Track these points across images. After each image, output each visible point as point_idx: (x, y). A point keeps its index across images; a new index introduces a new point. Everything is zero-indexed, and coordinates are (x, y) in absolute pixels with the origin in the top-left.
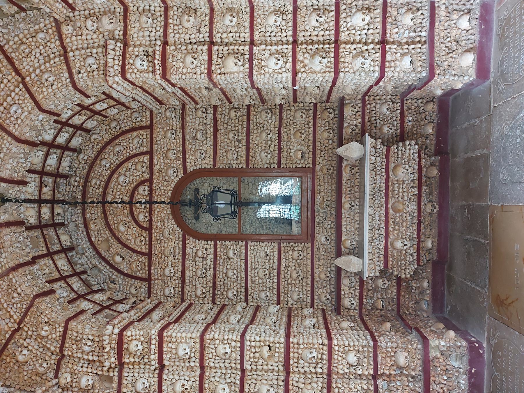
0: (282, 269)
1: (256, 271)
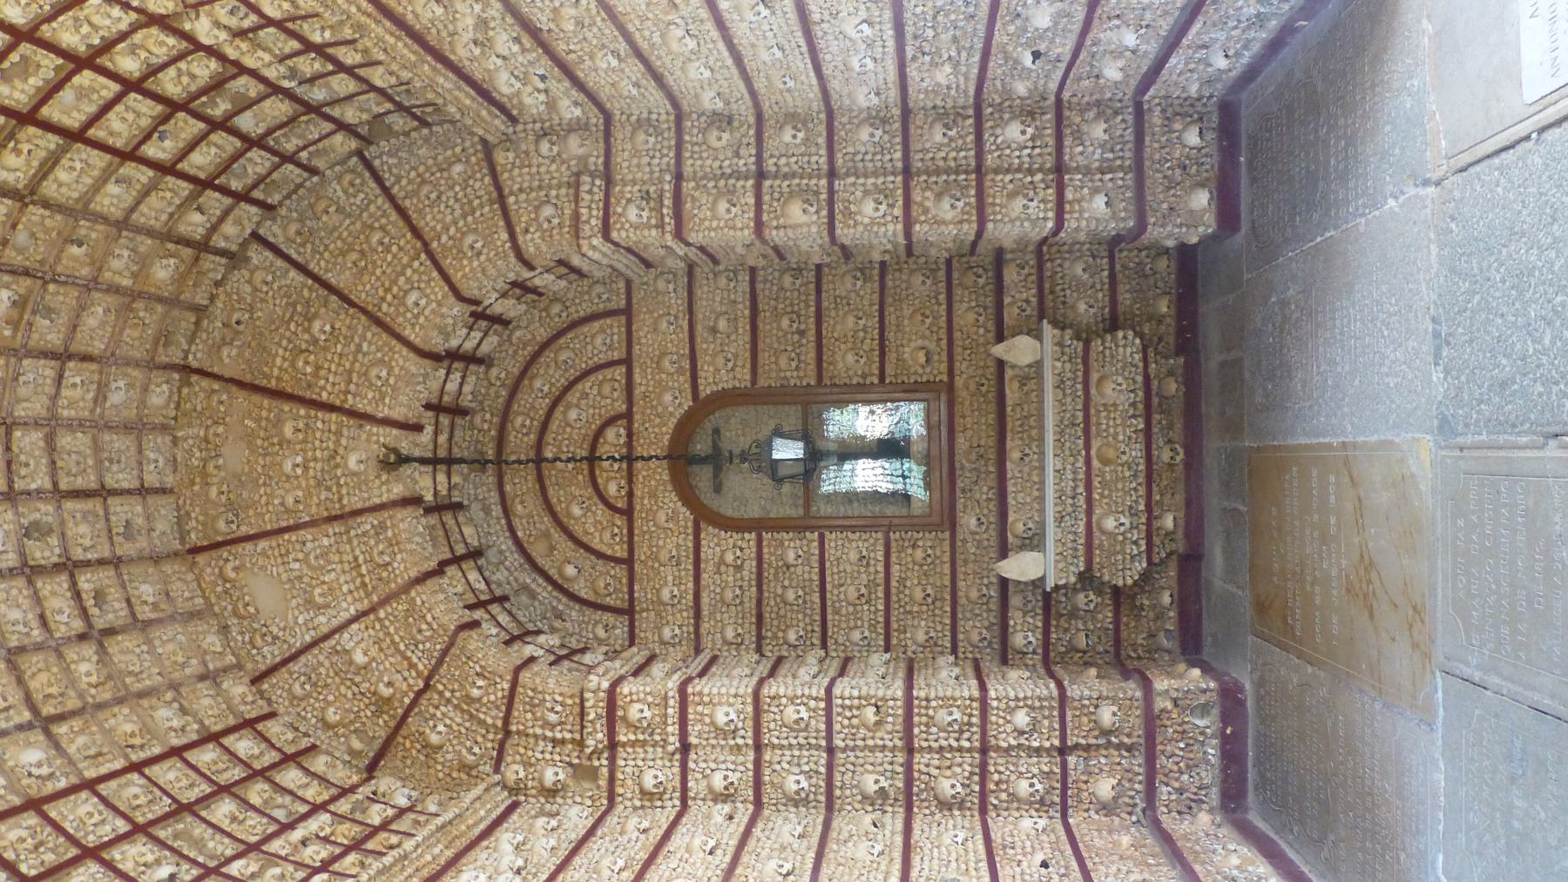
0: (894, 584)
1: (842, 589)
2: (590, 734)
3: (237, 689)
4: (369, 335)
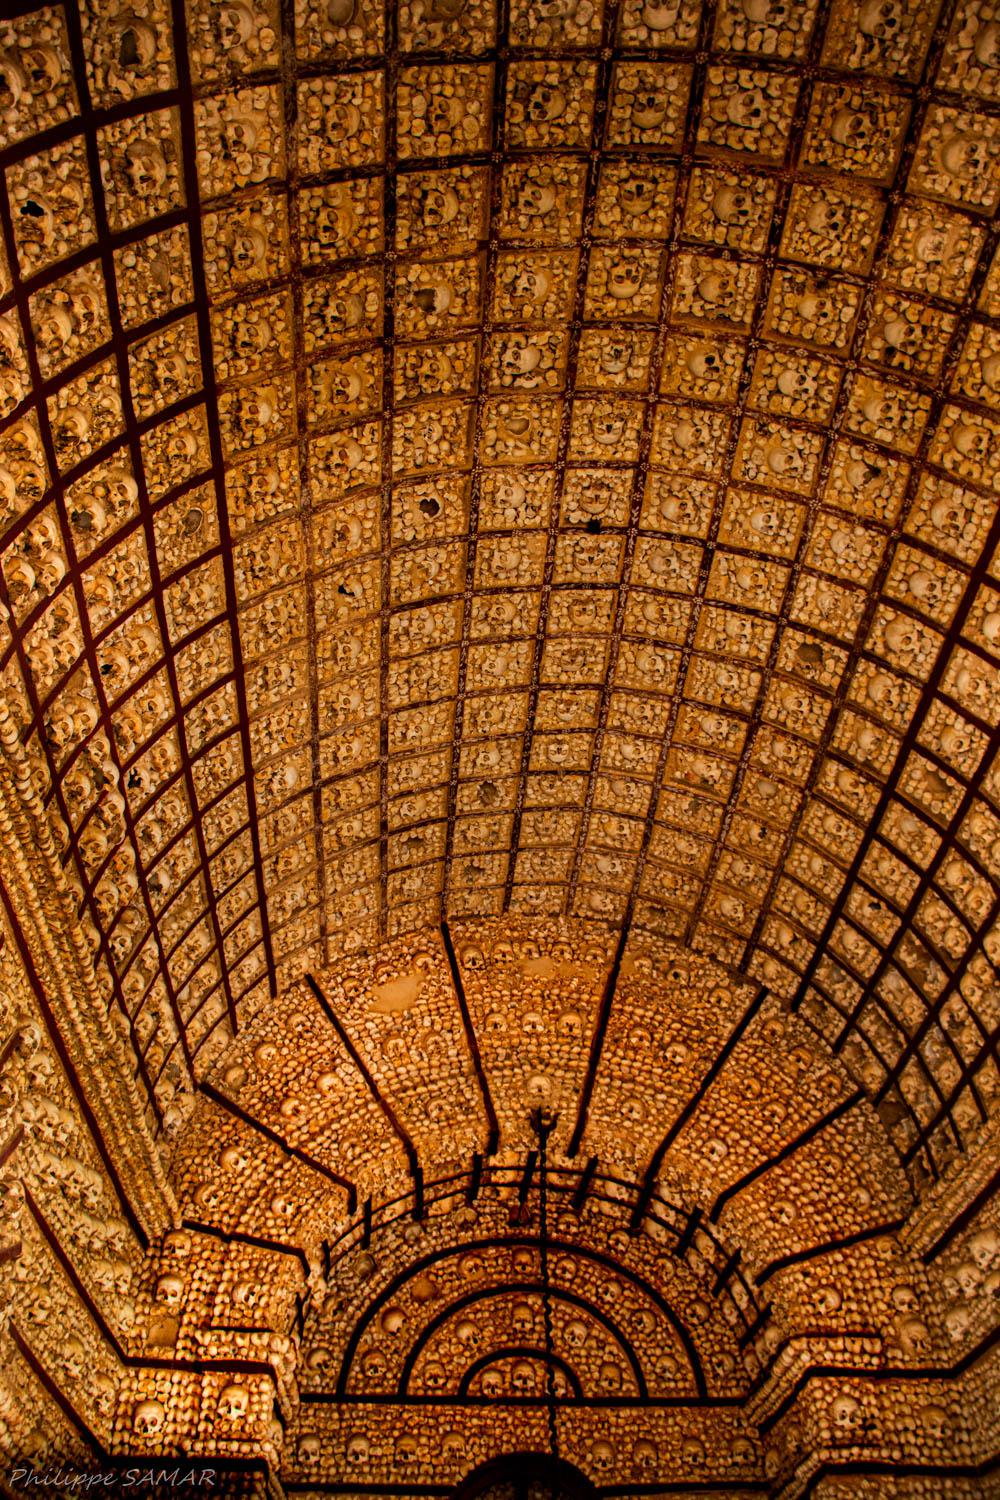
2: (219, 1339)
3: (305, 963)
4: (674, 1101)
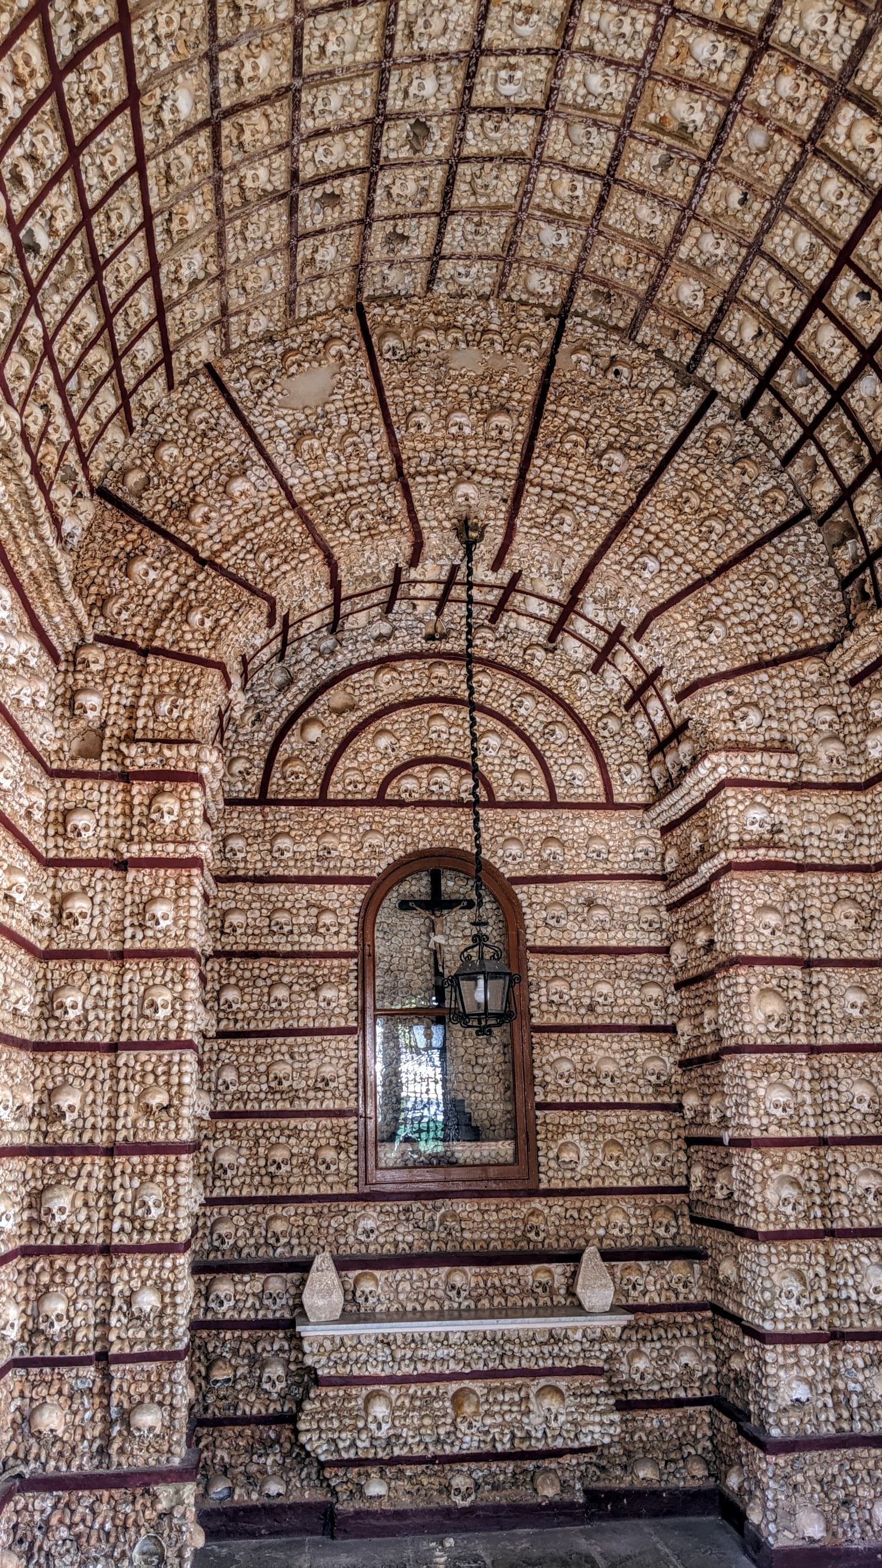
0: (293, 1122)
3: (205, 348)
4: (607, 514)
